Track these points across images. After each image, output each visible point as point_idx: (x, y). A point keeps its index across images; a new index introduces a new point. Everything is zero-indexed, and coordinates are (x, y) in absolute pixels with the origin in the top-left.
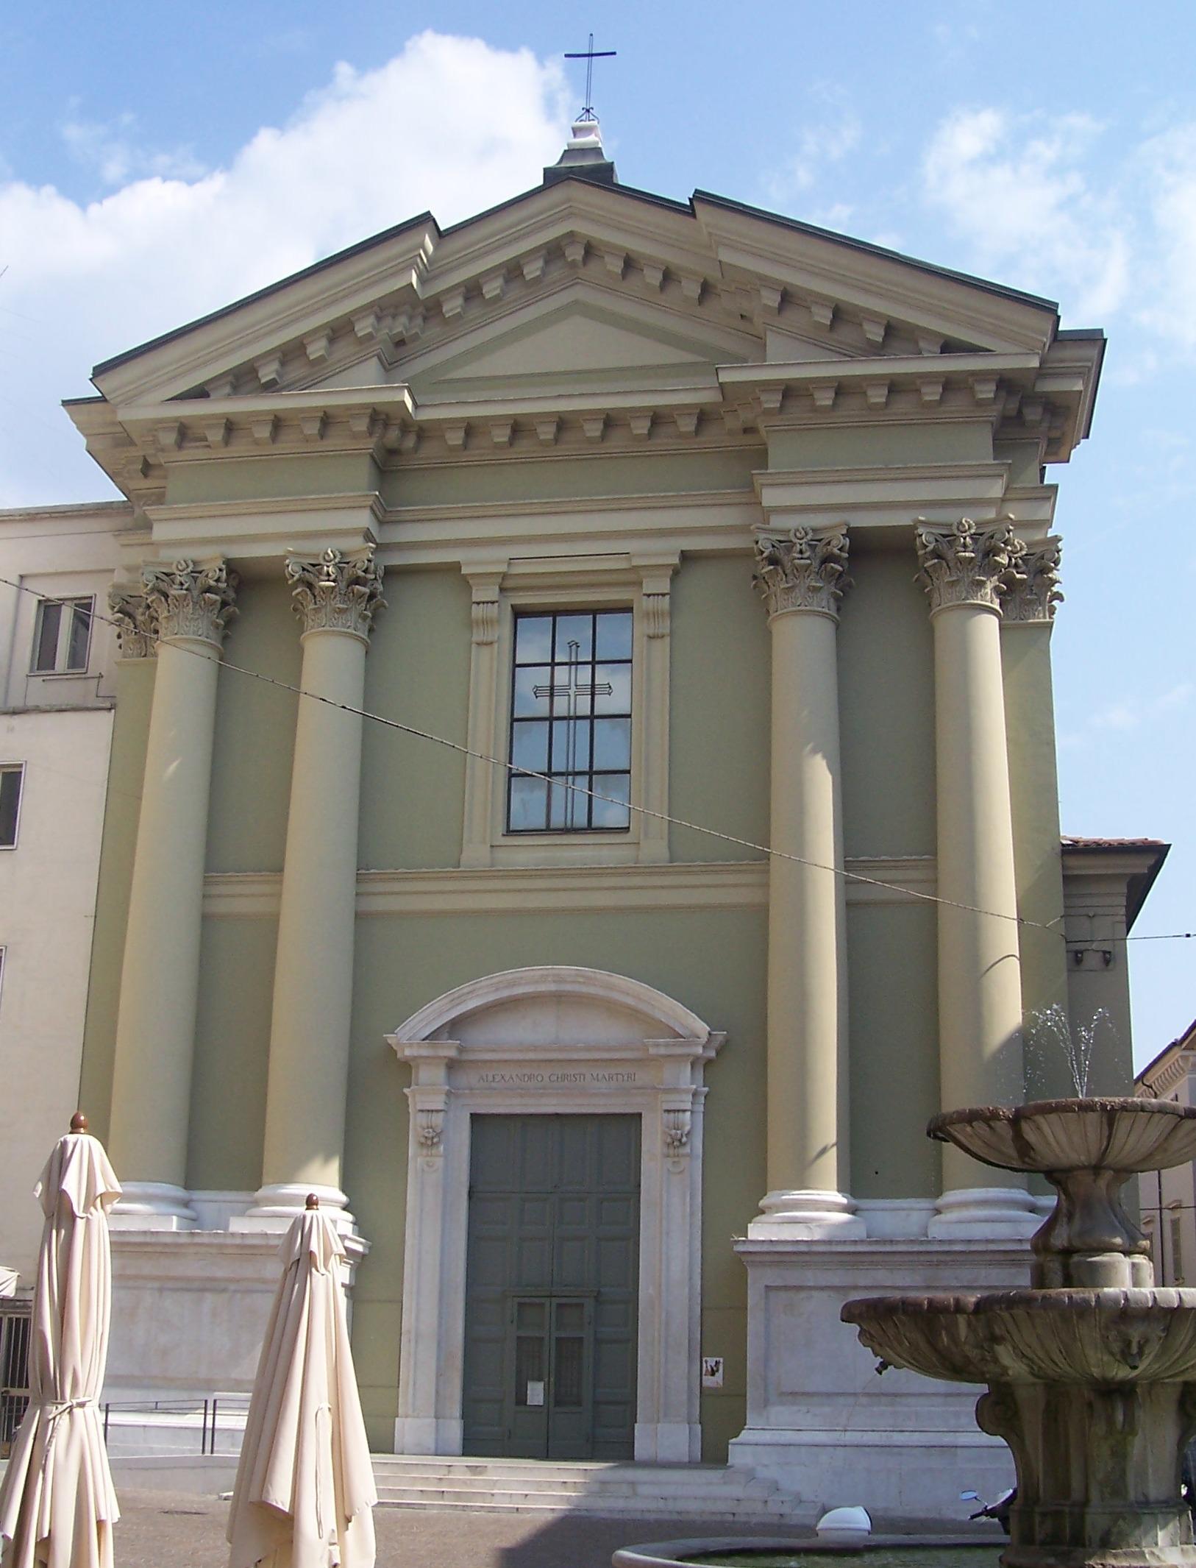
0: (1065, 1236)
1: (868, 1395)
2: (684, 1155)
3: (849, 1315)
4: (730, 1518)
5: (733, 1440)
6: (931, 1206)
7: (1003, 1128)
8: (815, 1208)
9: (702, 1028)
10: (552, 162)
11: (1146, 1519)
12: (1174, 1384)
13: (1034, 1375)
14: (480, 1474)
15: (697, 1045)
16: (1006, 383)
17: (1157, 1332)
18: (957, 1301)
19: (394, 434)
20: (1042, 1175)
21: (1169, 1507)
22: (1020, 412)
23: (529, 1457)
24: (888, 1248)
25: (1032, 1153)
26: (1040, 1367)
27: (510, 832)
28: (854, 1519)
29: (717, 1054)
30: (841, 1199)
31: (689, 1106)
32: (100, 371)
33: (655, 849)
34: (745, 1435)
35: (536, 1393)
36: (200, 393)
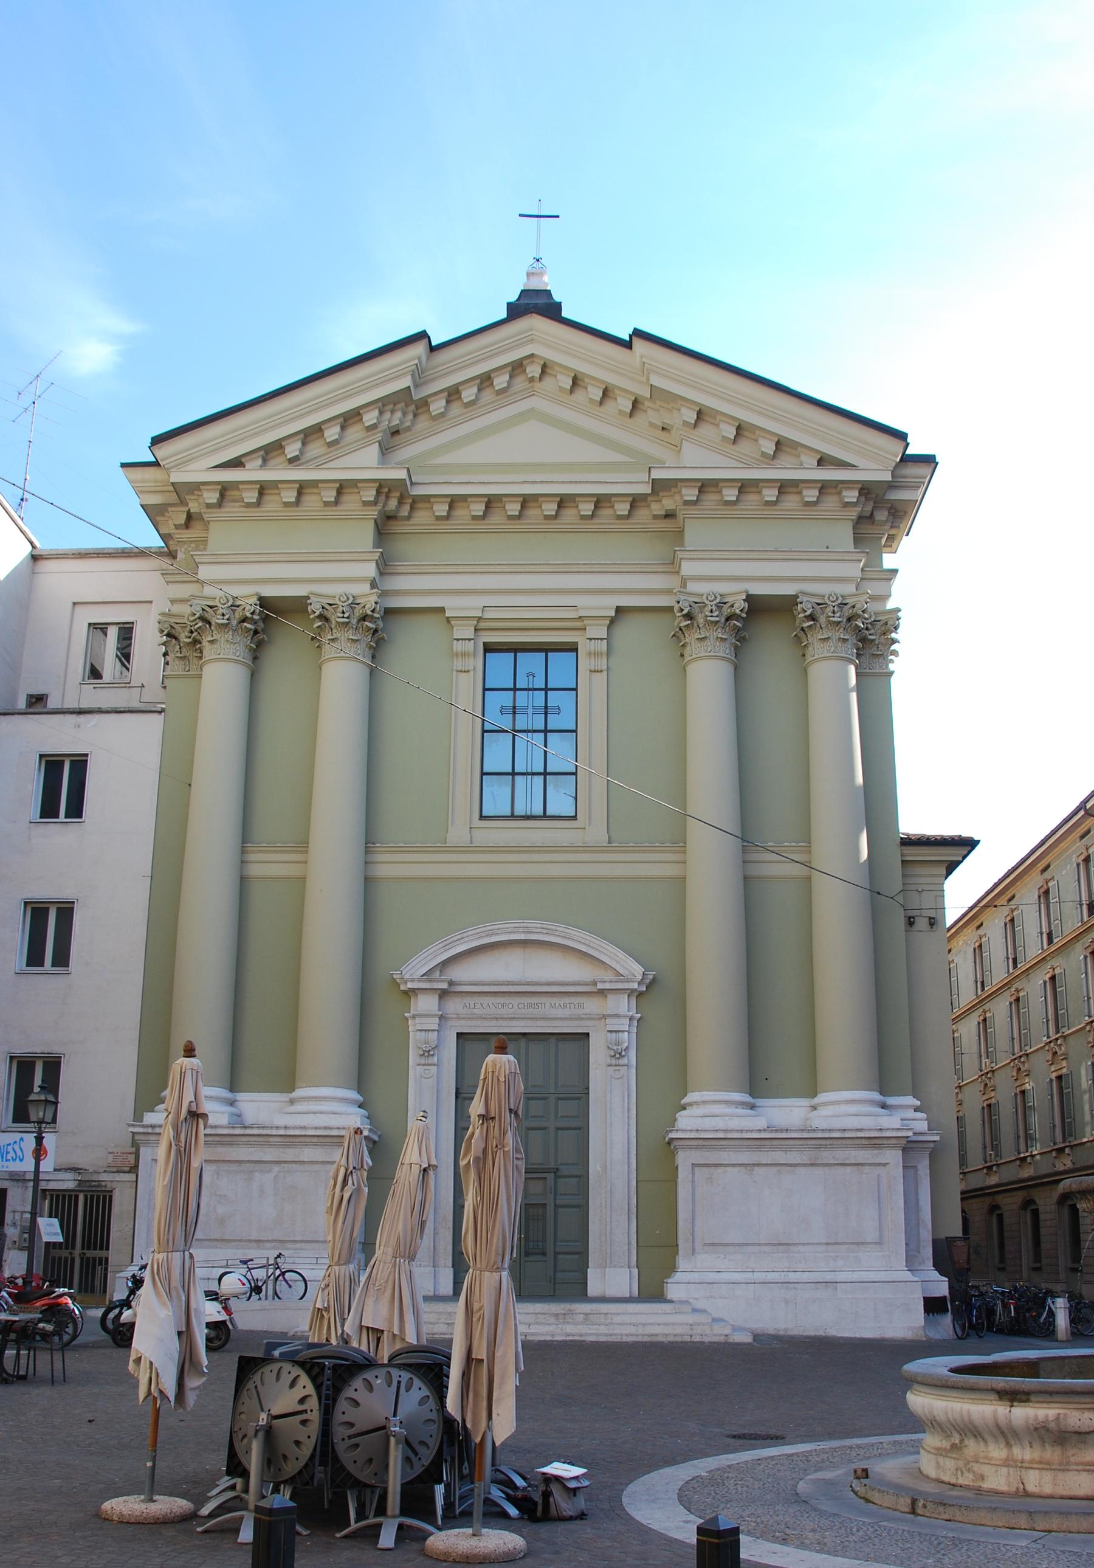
4: (688, 1339)
5: (669, 1281)
6: (808, 1104)
9: (638, 970)
10: (513, 298)
16: (866, 490)
19: (393, 504)
22: (872, 514)
27: (482, 817)
32: (157, 441)
33: (597, 833)
34: (678, 1276)
36: (236, 463)
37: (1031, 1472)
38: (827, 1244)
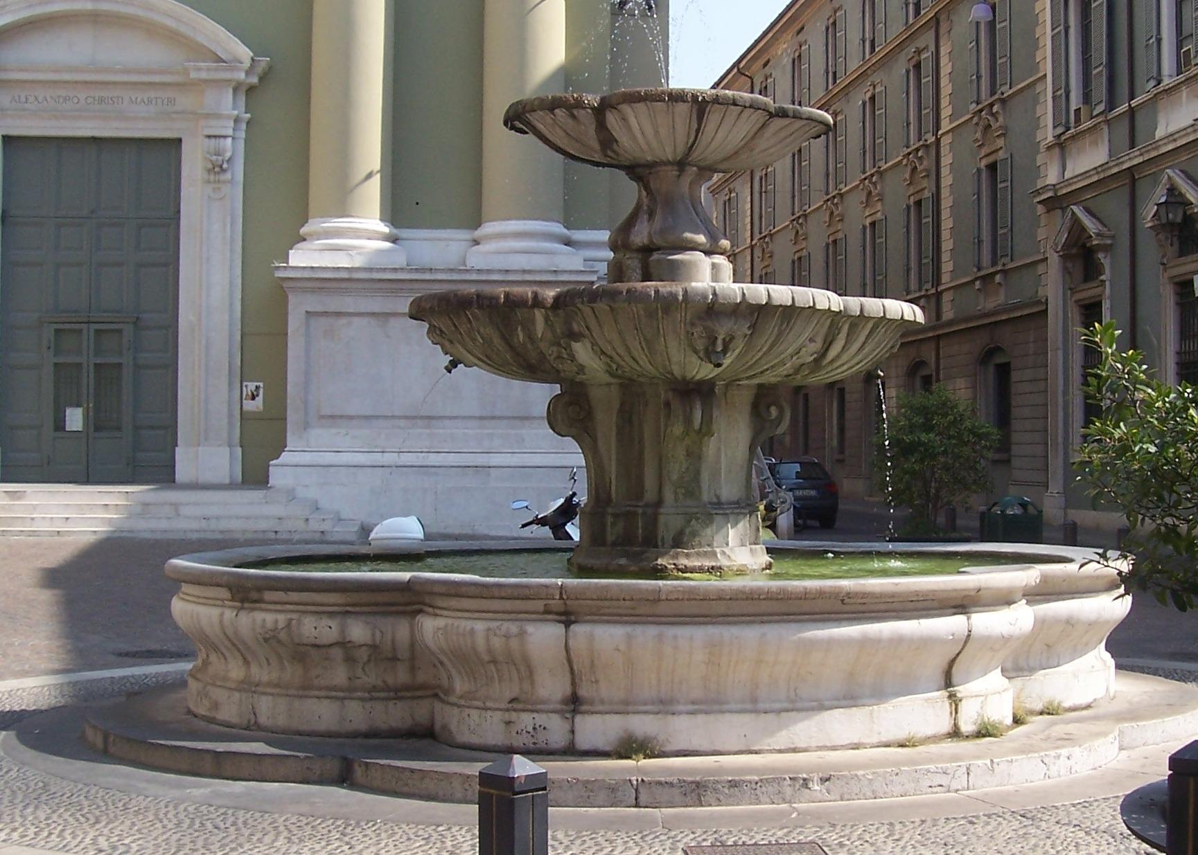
0: (646, 233)
1: (406, 417)
2: (224, 182)
3: (417, 313)
7: (585, 116)
8: (354, 236)
9: (245, 53)
11: (718, 519)
12: (748, 386)
13: (612, 375)
14: (19, 499)
15: (238, 69)
17: (743, 328)
18: (536, 295)
20: (622, 174)
21: (742, 507)
23: (70, 482)
24: (427, 276)
25: (615, 146)
26: (618, 365)
28: (405, 528)
29: (261, 79)
30: (385, 229)
31: (230, 132)
34: (285, 457)
35: (75, 419)
37: (264, 698)
38: (481, 418)
